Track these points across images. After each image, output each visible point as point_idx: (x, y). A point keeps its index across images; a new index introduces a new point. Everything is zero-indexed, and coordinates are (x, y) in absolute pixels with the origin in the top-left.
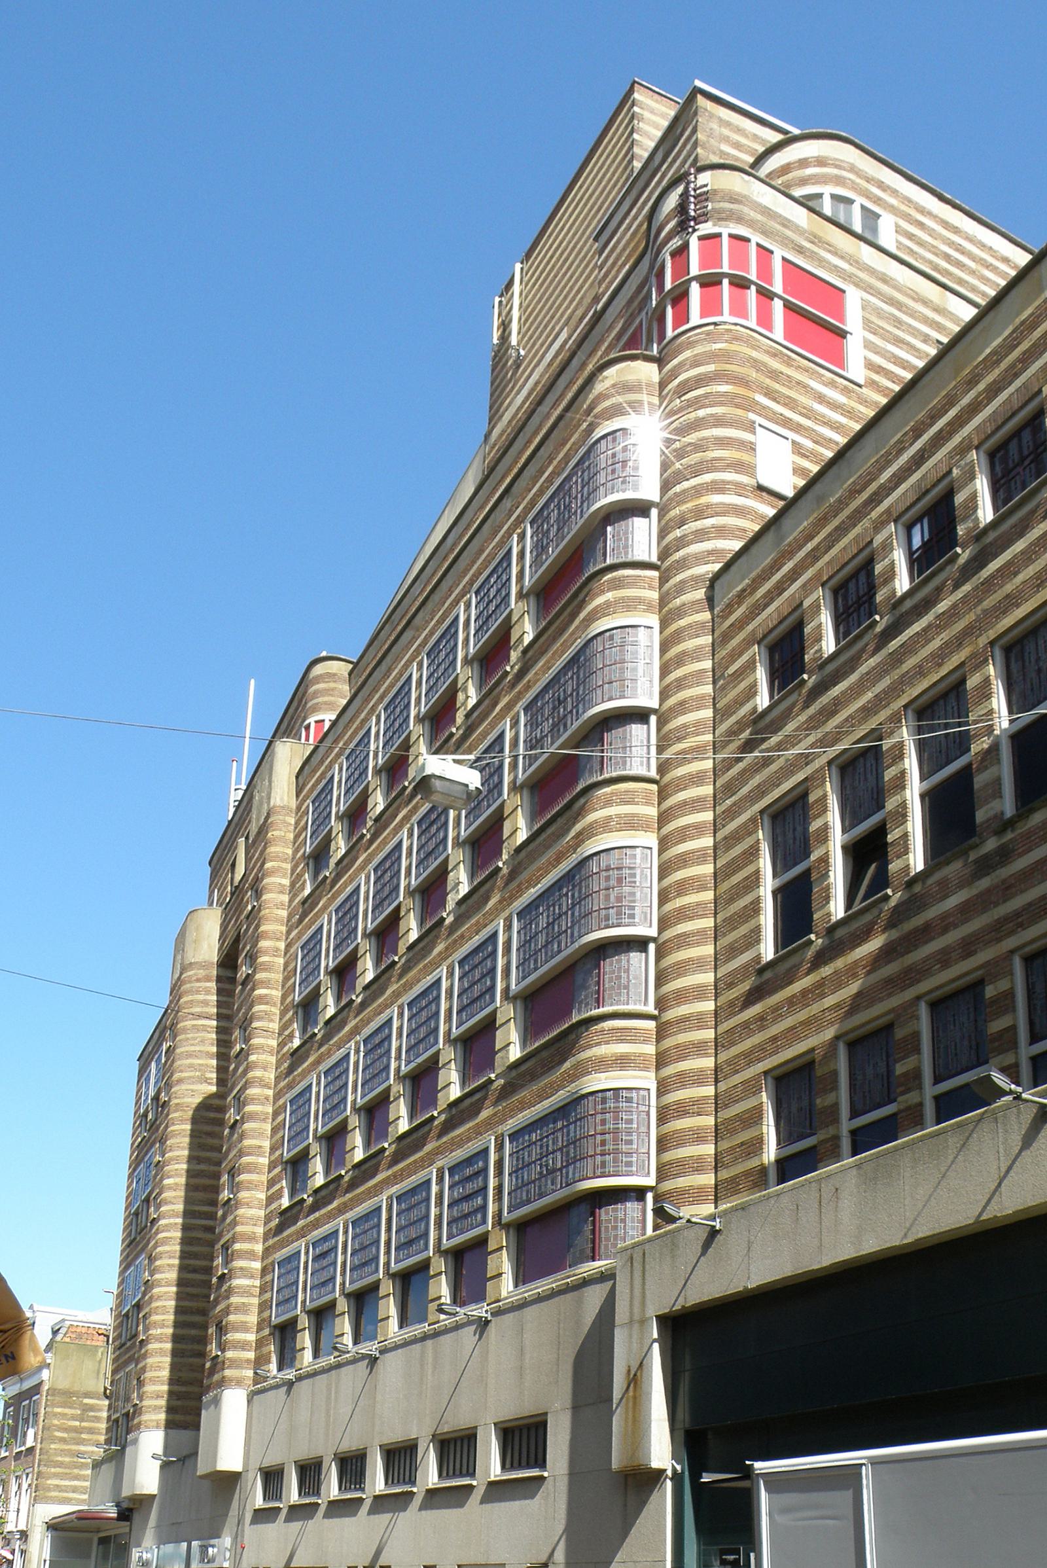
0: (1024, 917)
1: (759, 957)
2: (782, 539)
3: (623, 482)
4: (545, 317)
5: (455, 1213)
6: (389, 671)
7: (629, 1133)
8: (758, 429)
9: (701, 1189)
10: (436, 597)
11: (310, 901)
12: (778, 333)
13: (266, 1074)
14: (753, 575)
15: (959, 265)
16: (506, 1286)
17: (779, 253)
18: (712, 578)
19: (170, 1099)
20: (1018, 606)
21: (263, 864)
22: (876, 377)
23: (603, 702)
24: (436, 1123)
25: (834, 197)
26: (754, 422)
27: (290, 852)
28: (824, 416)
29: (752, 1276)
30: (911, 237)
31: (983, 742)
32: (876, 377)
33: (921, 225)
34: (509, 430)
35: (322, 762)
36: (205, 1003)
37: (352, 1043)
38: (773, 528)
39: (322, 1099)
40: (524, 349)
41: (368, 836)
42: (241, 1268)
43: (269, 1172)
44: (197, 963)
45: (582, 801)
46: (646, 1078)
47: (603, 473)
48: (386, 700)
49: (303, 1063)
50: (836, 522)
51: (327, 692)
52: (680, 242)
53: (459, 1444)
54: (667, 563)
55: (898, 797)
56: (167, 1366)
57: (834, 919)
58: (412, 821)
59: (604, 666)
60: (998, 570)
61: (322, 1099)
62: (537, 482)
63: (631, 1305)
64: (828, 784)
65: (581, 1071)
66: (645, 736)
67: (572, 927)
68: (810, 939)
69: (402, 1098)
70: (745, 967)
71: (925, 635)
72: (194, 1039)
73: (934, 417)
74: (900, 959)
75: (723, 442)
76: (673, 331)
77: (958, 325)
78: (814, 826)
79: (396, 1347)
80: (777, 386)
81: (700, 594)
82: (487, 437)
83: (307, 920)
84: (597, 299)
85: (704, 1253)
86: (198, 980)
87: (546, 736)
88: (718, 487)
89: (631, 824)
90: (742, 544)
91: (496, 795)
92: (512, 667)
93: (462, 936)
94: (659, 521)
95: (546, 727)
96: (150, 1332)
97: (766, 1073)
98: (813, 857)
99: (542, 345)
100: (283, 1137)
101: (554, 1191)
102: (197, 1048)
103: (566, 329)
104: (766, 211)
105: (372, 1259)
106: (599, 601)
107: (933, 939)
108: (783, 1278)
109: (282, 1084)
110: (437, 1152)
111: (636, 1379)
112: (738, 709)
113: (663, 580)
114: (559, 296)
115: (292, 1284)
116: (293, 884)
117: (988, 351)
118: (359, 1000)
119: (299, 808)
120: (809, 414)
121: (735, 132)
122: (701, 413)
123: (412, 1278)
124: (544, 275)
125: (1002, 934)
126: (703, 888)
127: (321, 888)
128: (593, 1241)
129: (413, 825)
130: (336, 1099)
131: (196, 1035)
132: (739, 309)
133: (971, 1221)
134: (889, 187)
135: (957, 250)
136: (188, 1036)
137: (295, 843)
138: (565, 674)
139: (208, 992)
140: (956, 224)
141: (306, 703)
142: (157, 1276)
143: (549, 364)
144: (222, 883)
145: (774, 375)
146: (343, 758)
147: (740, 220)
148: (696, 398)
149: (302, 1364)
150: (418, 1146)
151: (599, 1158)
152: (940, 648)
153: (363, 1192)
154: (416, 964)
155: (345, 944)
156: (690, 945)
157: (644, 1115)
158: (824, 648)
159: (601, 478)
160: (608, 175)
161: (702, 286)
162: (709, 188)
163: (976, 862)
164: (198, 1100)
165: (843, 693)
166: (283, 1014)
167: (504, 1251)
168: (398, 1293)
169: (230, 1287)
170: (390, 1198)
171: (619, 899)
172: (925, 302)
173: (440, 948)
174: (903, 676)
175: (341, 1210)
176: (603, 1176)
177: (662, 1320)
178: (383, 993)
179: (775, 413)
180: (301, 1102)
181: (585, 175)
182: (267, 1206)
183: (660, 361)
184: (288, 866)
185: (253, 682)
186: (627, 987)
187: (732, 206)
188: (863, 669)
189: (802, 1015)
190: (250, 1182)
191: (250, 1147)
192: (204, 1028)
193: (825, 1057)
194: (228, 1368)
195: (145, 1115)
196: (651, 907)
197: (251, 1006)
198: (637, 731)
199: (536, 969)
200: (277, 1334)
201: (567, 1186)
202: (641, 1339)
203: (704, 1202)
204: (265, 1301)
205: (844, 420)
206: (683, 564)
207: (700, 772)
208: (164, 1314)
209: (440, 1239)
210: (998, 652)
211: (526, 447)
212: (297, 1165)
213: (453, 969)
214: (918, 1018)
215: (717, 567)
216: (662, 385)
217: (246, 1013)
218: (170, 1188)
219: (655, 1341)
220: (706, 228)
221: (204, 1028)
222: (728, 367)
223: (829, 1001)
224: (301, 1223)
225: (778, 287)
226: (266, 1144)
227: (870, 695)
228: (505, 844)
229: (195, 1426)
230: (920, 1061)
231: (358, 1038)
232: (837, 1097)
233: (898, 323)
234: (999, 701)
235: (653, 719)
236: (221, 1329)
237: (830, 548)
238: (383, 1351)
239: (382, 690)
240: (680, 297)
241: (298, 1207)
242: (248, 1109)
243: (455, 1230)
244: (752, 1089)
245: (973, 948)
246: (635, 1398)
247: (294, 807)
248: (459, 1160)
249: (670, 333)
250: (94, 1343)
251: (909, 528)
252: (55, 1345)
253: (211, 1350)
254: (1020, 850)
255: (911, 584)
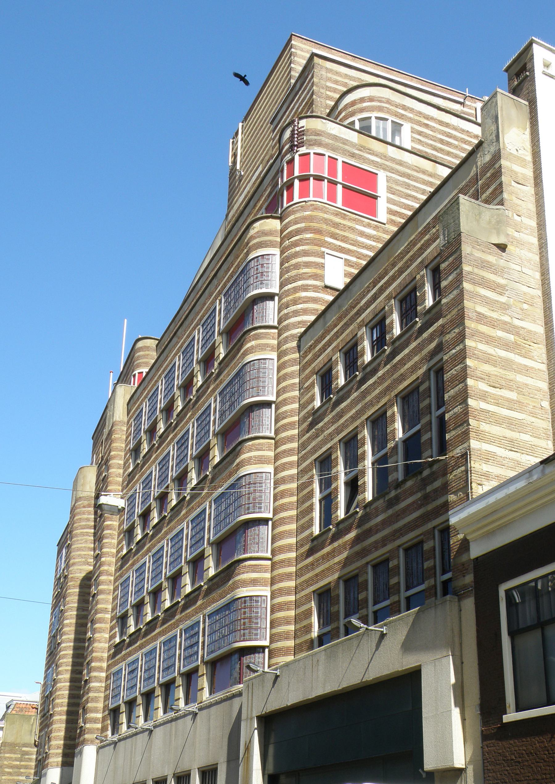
0: (403, 531)
1: (312, 533)
2: (325, 324)
3: (261, 284)
4: (252, 156)
5: (186, 654)
6: (167, 357)
7: (257, 619)
8: (326, 255)
9: (288, 648)
10: (187, 323)
11: (131, 475)
12: (339, 203)
13: (110, 568)
14: (315, 339)
15: (448, 144)
16: (205, 695)
17: (340, 159)
18: (300, 335)
19: (68, 574)
20: (405, 380)
21: (110, 452)
22: (394, 218)
23: (249, 398)
24: (180, 605)
25: (377, 118)
26: (324, 252)
27: (124, 446)
28: (363, 243)
29: (290, 700)
30: (420, 133)
31: (392, 443)
32: (394, 218)
33: (427, 126)
34: (236, 215)
35: (138, 399)
36: (88, 520)
37: (147, 557)
38: (323, 316)
39: (134, 585)
40: (243, 171)
41: (157, 445)
42: (95, 677)
43: (111, 623)
44: (83, 497)
45: (239, 447)
46: (266, 590)
47: (252, 278)
48: (166, 373)
49: (127, 564)
50: (345, 321)
51: (145, 356)
52: (290, 157)
53: (185, 777)
54: (280, 327)
55: (362, 463)
56: (63, 729)
57: (339, 519)
58: (216, 393)
59: (250, 379)
60: (399, 361)
61: (134, 585)
62: (227, 274)
63: (248, 710)
64: (339, 451)
65: (235, 587)
66: (270, 414)
67: (234, 512)
68: (356, 511)
69: (167, 590)
70: (307, 537)
71: (409, 357)
72: (82, 540)
73: (381, 278)
74: (361, 544)
75: (307, 265)
76: (287, 204)
77: (404, 219)
78: (360, 451)
79: (161, 725)
80: (337, 231)
81: (294, 344)
82: (227, 216)
83: (130, 485)
84: (271, 157)
85: (273, 686)
86: (84, 507)
87: (227, 410)
88: (305, 288)
89: (261, 460)
90: (316, 317)
91: (207, 436)
92: (215, 370)
93: (193, 508)
94: (279, 303)
95: (228, 404)
96: (55, 709)
97: (314, 592)
98: (332, 487)
99: (251, 171)
100: (117, 603)
101: (224, 647)
102: (83, 545)
103: (261, 165)
104: (335, 138)
105: (172, 665)
106: (249, 345)
107: (372, 536)
108: (299, 702)
109: (118, 574)
110: (180, 621)
111: (248, 748)
112: (308, 406)
113: (279, 335)
114: (252, 156)
115: (172, 656)
116: (125, 464)
117: (399, 251)
118: (151, 533)
119: (128, 422)
120: (355, 243)
121: (334, 75)
122: (298, 249)
123: (193, 676)
124: (259, 121)
125: (395, 537)
126: (292, 495)
127: (136, 470)
128: (240, 674)
129: (174, 443)
130: (140, 586)
131: (83, 538)
132: (318, 194)
133: (359, 682)
134: (408, 108)
135: (447, 136)
136: (79, 538)
137: (126, 441)
138: (235, 380)
139: (89, 513)
140: (447, 122)
141: (134, 362)
142: (59, 677)
143: (253, 183)
144: (97, 452)
145: (336, 225)
146: (181, 353)
147: (320, 144)
148: (296, 241)
149: (121, 732)
150: (173, 616)
151: (242, 631)
152: (379, 394)
153: (150, 638)
154: (174, 518)
155: (146, 501)
156: (285, 524)
157: (264, 610)
158: (339, 383)
159: (251, 281)
160: (280, 84)
161: (300, 181)
162: (305, 128)
163: (388, 501)
164: (83, 575)
165: (345, 407)
166: (119, 535)
167: (205, 676)
168: (127, 711)
169: (89, 687)
170: (160, 643)
171: (254, 499)
172: (424, 172)
173: (184, 512)
174: (366, 404)
175: (141, 647)
176: (244, 640)
177: (259, 718)
178: (161, 531)
179: (335, 245)
180: (177, 540)
181: (270, 80)
182: (110, 641)
183: (281, 219)
184: (123, 454)
185: (126, 320)
186: (258, 544)
187: (316, 138)
188: (352, 397)
189: (327, 565)
190: (100, 628)
191: (101, 609)
192: (87, 534)
193: (335, 587)
194: (87, 733)
195: (60, 578)
196: (270, 503)
197: (103, 531)
198: (266, 412)
199: (220, 531)
200: (112, 714)
201: (229, 644)
202: (251, 727)
203: (289, 654)
204: (107, 695)
205: (374, 244)
206: (287, 328)
207: (292, 435)
208: (62, 699)
209: (180, 667)
210: (399, 400)
211: (231, 243)
212: (123, 619)
213: (189, 524)
214: (367, 573)
215: (303, 330)
216: (282, 231)
217: (101, 534)
218: (67, 625)
219: (255, 729)
220: (303, 150)
221: (87, 534)
222: (311, 224)
223: (337, 560)
224: (123, 653)
225: (339, 179)
226: (110, 607)
227: (354, 411)
228: (210, 463)
229: (71, 764)
230: (367, 594)
231: (150, 554)
232: (339, 608)
233: (408, 186)
234: (398, 425)
235: (273, 406)
236: (85, 711)
237: (343, 333)
238: (155, 727)
239: (164, 367)
240: (290, 186)
241: (122, 644)
242: (101, 587)
243: (186, 663)
244: (307, 599)
245: (386, 543)
246: (247, 758)
247: (126, 421)
248: (189, 625)
249: (285, 205)
250: (30, 714)
251: (372, 329)
252: (6, 716)
253: (80, 723)
254: (402, 498)
255: (372, 357)
